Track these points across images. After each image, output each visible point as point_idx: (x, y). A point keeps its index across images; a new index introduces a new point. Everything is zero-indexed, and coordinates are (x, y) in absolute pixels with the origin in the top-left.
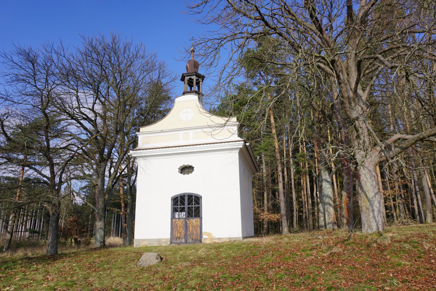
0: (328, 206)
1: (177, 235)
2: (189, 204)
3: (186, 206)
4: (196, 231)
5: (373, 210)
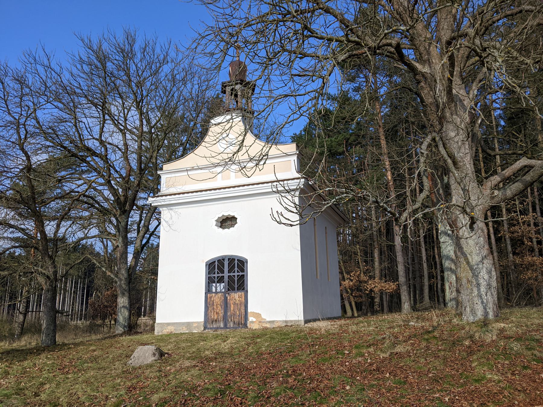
0: (449, 273)
1: (213, 317)
3: (226, 274)
4: (240, 310)
5: (478, 285)
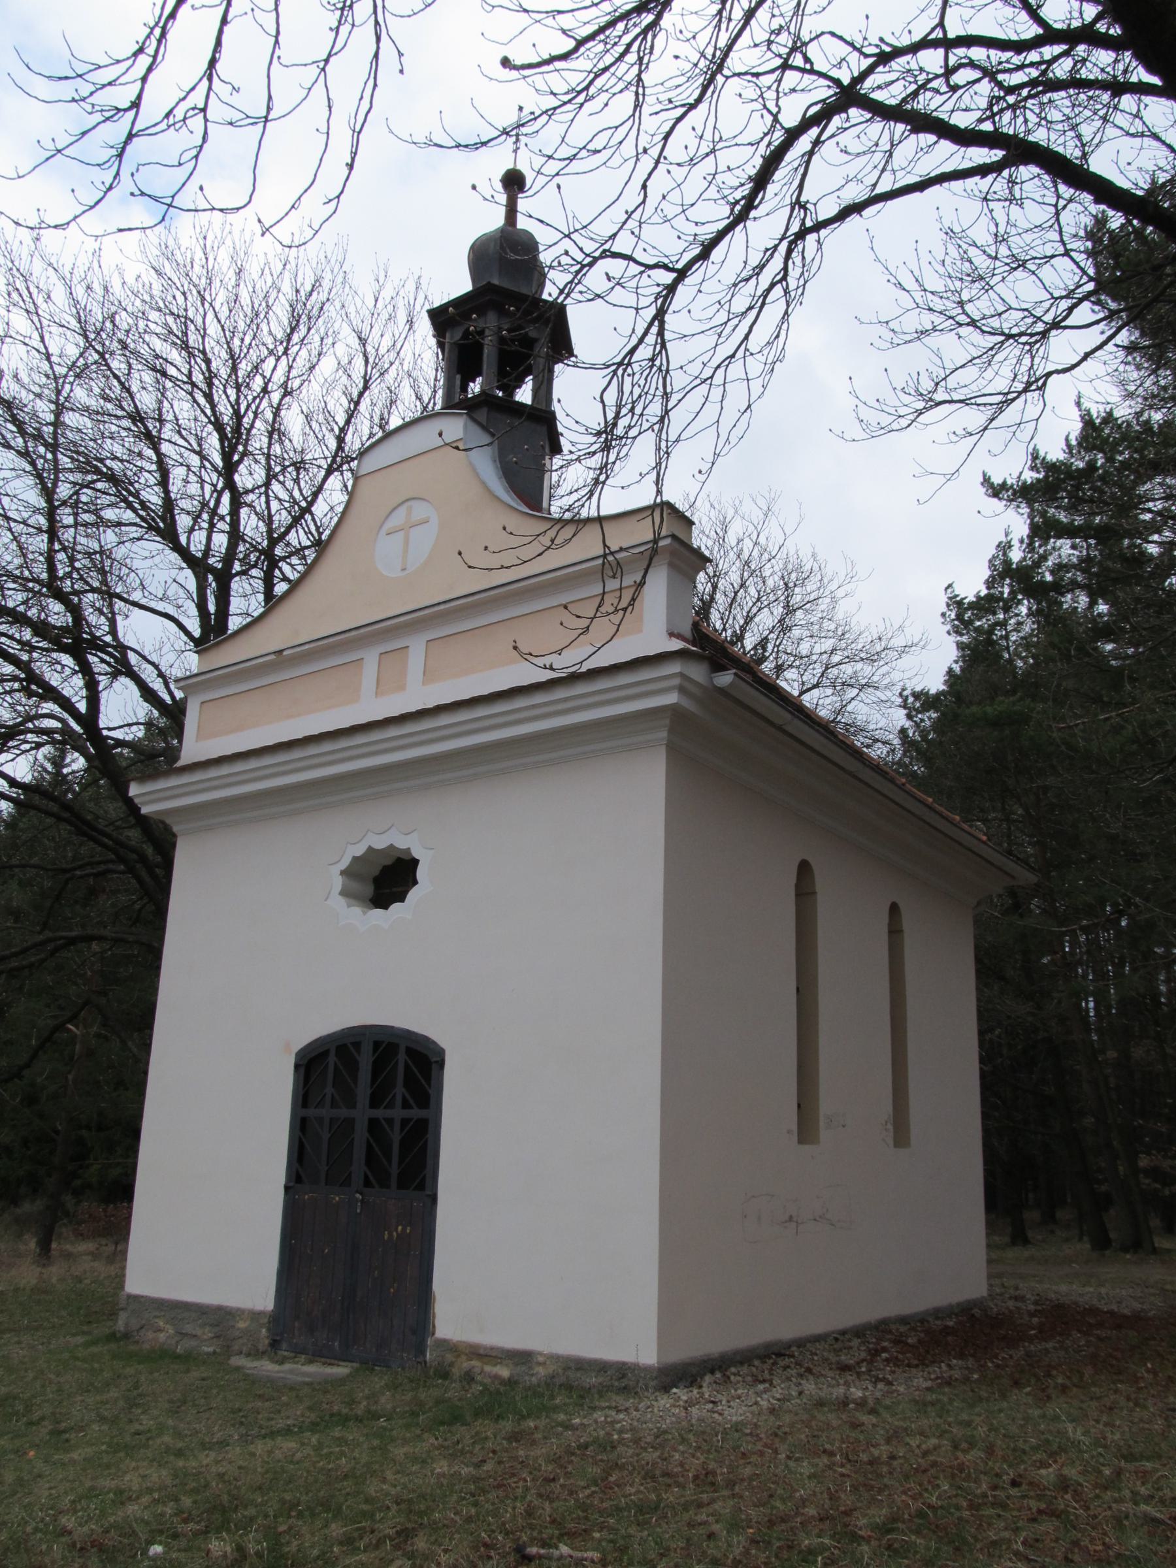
2: (374, 1103)
